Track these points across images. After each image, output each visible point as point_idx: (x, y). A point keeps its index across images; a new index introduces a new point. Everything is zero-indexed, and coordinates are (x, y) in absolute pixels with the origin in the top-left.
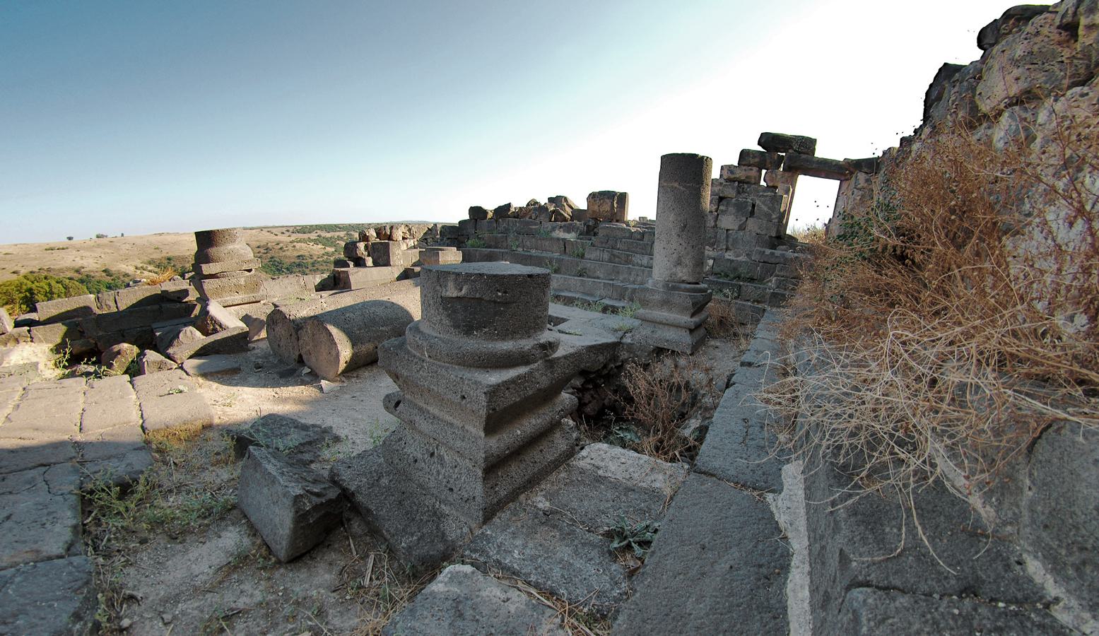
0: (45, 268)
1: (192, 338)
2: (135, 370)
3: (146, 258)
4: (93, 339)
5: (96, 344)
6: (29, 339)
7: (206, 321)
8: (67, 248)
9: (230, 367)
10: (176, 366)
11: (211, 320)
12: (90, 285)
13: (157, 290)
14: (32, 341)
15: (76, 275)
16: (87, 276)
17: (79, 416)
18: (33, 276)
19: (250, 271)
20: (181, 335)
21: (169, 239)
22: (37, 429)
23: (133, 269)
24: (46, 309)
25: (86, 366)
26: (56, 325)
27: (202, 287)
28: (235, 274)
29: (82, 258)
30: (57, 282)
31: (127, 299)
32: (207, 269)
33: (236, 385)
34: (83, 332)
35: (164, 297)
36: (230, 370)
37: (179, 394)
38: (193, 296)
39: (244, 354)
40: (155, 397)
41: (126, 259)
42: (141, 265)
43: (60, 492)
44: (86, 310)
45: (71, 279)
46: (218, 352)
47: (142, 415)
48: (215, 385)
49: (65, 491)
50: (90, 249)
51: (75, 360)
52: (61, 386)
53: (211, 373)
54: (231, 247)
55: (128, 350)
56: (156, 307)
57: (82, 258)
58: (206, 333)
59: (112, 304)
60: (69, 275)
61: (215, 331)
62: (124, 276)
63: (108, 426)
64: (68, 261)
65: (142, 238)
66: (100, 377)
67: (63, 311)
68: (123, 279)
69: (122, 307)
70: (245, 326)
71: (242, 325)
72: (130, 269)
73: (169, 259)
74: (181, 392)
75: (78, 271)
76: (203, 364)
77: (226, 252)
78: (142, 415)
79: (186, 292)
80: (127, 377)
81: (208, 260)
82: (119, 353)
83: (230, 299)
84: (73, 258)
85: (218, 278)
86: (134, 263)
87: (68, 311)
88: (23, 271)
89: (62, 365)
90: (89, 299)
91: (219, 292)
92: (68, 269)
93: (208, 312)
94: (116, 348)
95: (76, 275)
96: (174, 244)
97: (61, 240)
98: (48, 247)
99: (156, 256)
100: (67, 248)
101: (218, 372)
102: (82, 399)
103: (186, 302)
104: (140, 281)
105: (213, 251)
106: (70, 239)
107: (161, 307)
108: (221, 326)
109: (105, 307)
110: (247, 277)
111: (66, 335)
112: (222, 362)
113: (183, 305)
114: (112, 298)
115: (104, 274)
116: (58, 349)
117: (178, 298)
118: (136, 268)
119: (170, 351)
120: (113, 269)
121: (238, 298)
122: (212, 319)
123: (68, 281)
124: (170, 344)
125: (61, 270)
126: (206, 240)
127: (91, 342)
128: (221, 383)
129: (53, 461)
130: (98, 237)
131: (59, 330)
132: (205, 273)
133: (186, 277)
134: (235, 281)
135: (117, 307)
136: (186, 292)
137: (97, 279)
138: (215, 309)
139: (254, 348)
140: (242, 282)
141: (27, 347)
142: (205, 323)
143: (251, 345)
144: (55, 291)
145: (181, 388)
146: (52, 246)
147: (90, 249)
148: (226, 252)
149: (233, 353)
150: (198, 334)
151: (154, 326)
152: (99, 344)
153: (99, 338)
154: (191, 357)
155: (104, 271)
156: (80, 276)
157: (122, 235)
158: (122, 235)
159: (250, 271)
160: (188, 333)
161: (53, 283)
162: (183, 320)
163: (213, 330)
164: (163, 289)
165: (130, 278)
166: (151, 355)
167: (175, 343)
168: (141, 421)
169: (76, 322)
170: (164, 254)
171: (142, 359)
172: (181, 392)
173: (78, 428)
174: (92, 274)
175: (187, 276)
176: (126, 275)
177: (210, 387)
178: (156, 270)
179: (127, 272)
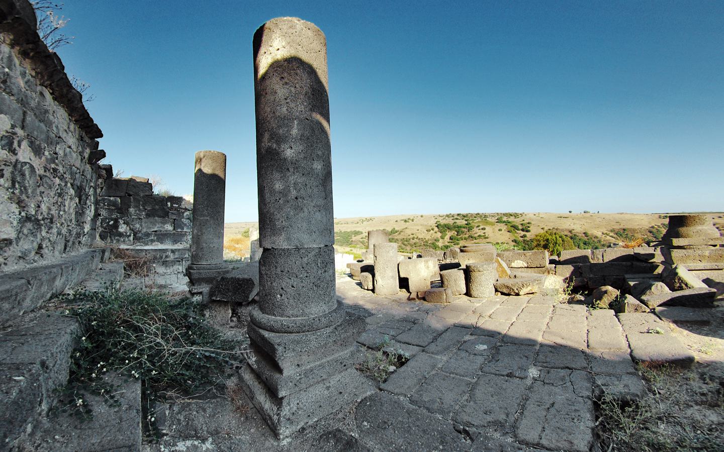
0: (556, 228)
1: (660, 292)
2: (618, 307)
3: (610, 228)
4: (587, 279)
5: (587, 282)
6: (554, 272)
7: (674, 280)
8: (568, 217)
9: (694, 319)
10: (649, 310)
11: (679, 280)
12: (575, 241)
13: (630, 252)
14: (555, 274)
15: (569, 234)
16: (575, 235)
17: (586, 335)
18: (550, 232)
19: (715, 246)
20: (653, 288)
21: (627, 217)
22: (563, 339)
23: (601, 234)
24: (566, 255)
25: (581, 296)
26: (564, 266)
27: (670, 254)
28: (700, 247)
29: (574, 224)
30: (560, 237)
31: (610, 255)
32: (676, 242)
33: (707, 335)
34: (582, 273)
35: (636, 257)
36: (694, 321)
37: (657, 334)
38: (659, 258)
39: (709, 310)
40: (636, 333)
41: (598, 227)
42: (606, 232)
43: (581, 395)
44: (585, 258)
45: (566, 236)
46: (683, 305)
47: (629, 345)
48: (686, 332)
49: (584, 395)
50: (579, 219)
51: (575, 291)
52: (572, 309)
53: (681, 321)
54: (699, 228)
55: (612, 292)
56: (629, 263)
57: (574, 224)
58: (673, 289)
59: (601, 257)
60: (566, 233)
61: (681, 288)
62: (594, 238)
63: (606, 348)
64: (566, 225)
65: (609, 215)
66: (595, 308)
67: (573, 257)
68: (594, 239)
69: (606, 260)
70: (707, 287)
71: (704, 286)
72: (599, 234)
73: (624, 230)
74: (658, 333)
75: (570, 232)
76: (665, 310)
77: (695, 231)
78: (629, 345)
79: (653, 256)
80: (613, 312)
81: (678, 235)
82: (606, 292)
83: (693, 265)
84: (569, 223)
85: (685, 249)
86: (602, 230)
87: (575, 258)
88: (546, 228)
89: (568, 292)
90: (588, 252)
91: (683, 259)
92: (566, 230)
93: (677, 274)
94: (604, 288)
95: (569, 234)
96: (629, 220)
97: (565, 212)
98: (559, 216)
99: (617, 227)
100: (568, 217)
101: (687, 322)
102: (586, 322)
103: (652, 262)
104: (618, 244)
105: (683, 230)
106: (570, 212)
107: (632, 264)
108: (686, 285)
109: (596, 258)
110: (713, 250)
111: (573, 273)
112: (689, 314)
113: (649, 265)
114: (601, 254)
115: (584, 235)
116: (568, 280)
117: (646, 259)
118: (603, 234)
119: (644, 297)
120: (589, 233)
121: (701, 265)
122: (680, 279)
123: (565, 237)
124: (643, 292)
125: (562, 230)
126: (678, 222)
127: (589, 283)
128: (690, 331)
129: (574, 366)
130: (584, 212)
131: (568, 270)
132: (674, 244)
133: (651, 245)
134: (700, 252)
135: (603, 260)
136: (653, 256)
137: (579, 237)
138: (682, 272)
139: (718, 306)
140: (707, 253)
141: (552, 277)
142: (671, 278)
143: (716, 303)
144: (558, 242)
145: (658, 329)
146: (561, 215)
147: (579, 219)
148: (695, 231)
149: (698, 307)
150: (666, 289)
151: (627, 276)
152: (589, 283)
153: (590, 279)
154: (658, 306)
155: (584, 233)
156: (571, 235)
157: (598, 212)
158: (598, 212)
159: (715, 246)
160: (659, 287)
161: (558, 237)
162: (648, 275)
163: (679, 287)
164: (636, 252)
165: (598, 239)
166: (630, 299)
167: (648, 292)
168: (629, 350)
169: (580, 266)
170: (622, 227)
171: (624, 301)
172: (658, 333)
173: (586, 345)
174: (577, 234)
175: (652, 244)
176: (596, 237)
177: (681, 333)
178: (615, 236)
179: (597, 235)
